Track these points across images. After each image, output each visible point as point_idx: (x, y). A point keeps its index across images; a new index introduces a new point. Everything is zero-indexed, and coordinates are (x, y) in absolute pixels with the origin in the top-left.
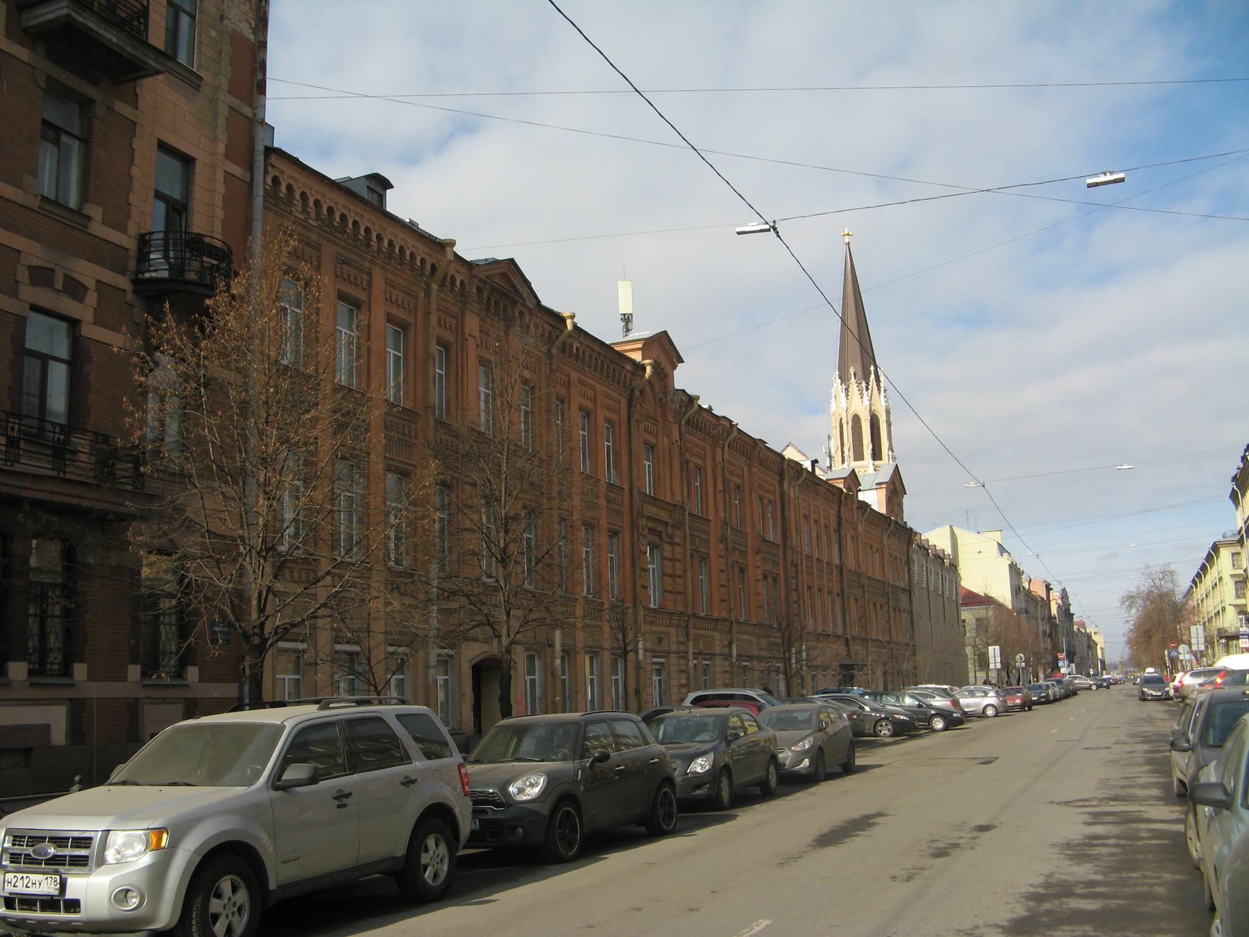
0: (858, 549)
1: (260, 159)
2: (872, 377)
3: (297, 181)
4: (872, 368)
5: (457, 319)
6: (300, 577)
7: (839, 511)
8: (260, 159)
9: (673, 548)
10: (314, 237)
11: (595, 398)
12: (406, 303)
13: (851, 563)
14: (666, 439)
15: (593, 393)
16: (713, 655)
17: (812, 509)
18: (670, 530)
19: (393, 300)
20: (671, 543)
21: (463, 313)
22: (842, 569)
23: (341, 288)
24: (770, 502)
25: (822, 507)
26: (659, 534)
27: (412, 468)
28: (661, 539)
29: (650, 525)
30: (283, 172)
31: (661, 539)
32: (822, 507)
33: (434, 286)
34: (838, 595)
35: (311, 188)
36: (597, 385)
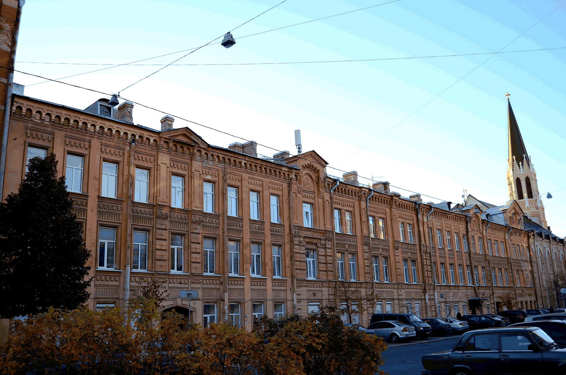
0: (484, 243)
1: (9, 100)
2: (525, 159)
3: (88, 120)
4: (524, 155)
5: (188, 164)
6: (276, 284)
7: (467, 226)
8: (9, 100)
9: (326, 250)
10: (49, 129)
11: (413, 220)
12: (344, 204)
13: (478, 249)
14: (320, 200)
15: (412, 218)
16: (393, 299)
17: (444, 226)
18: (323, 242)
19: (311, 197)
20: (325, 248)
21: (158, 154)
22: (470, 253)
23: (69, 149)
24: (410, 224)
25: (452, 224)
26: (316, 244)
27: (120, 225)
28: (317, 247)
29: (307, 240)
30: (52, 111)
31: (317, 247)
32: (452, 224)
33: (332, 192)
34: (467, 266)
35: (42, 109)
36: (263, 179)
